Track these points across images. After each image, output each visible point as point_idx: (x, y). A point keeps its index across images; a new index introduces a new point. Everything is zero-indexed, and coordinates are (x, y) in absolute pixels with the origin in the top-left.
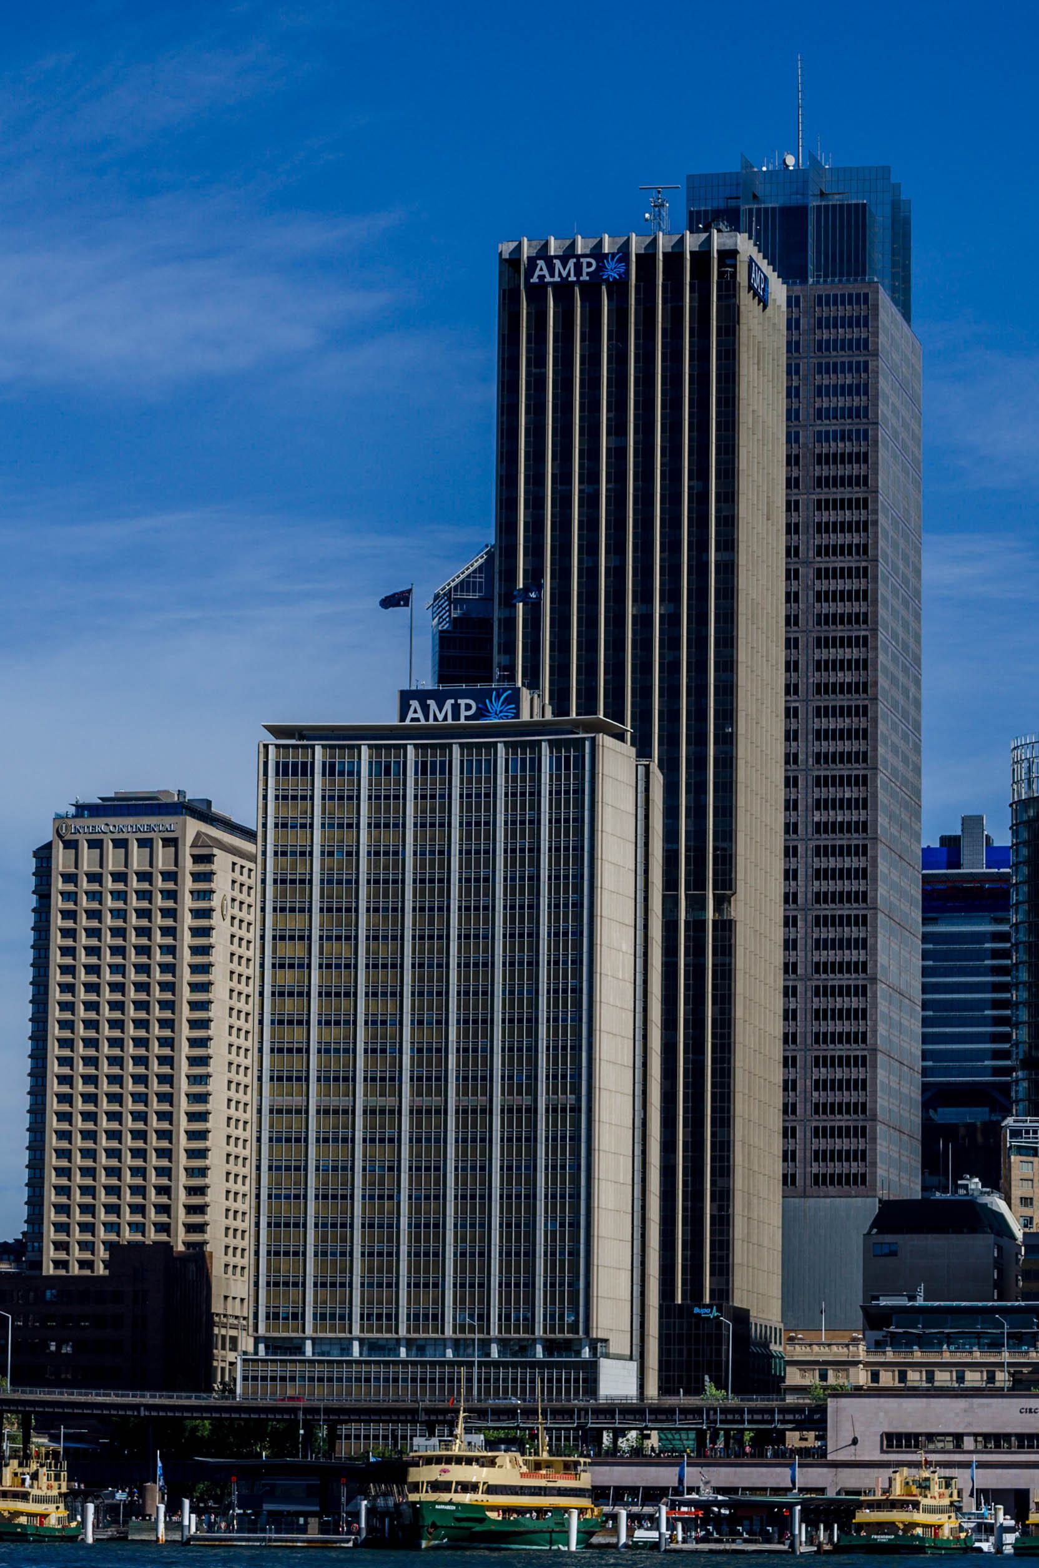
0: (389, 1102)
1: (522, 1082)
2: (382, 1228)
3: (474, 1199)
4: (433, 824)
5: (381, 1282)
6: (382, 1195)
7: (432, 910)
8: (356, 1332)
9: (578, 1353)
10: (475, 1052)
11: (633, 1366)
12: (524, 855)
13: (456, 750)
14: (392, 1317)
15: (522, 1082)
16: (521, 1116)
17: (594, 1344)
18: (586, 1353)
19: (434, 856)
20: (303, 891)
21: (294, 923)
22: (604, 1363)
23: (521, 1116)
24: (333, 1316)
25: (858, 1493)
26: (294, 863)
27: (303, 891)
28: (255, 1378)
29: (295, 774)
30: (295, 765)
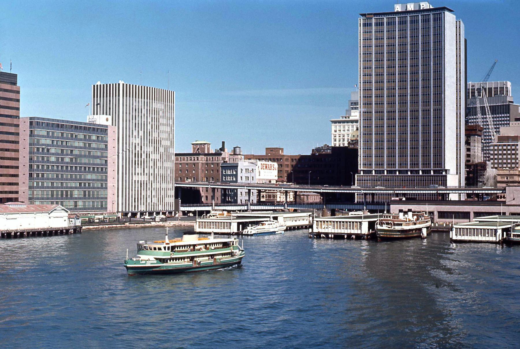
0: (428, 108)
1: (426, 103)
2: (391, 141)
3: (414, 133)
4: (403, 37)
5: (392, 155)
6: (391, 133)
7: (403, 59)
8: (432, 168)
9: (442, 173)
10: (414, 95)
11: (457, 176)
12: (426, 43)
13: (420, 16)
14: (394, 164)
15: (426, 103)
16: (426, 112)
17: (446, 171)
18: (444, 173)
19: (403, 45)
20: (370, 56)
21: (368, 64)
22: (448, 176)
23: (426, 112)
24: (379, 164)
25: (420, 212)
26: (368, 49)
27: (370, 56)
28: (360, 180)
29: (379, 25)
30: (368, 24)
